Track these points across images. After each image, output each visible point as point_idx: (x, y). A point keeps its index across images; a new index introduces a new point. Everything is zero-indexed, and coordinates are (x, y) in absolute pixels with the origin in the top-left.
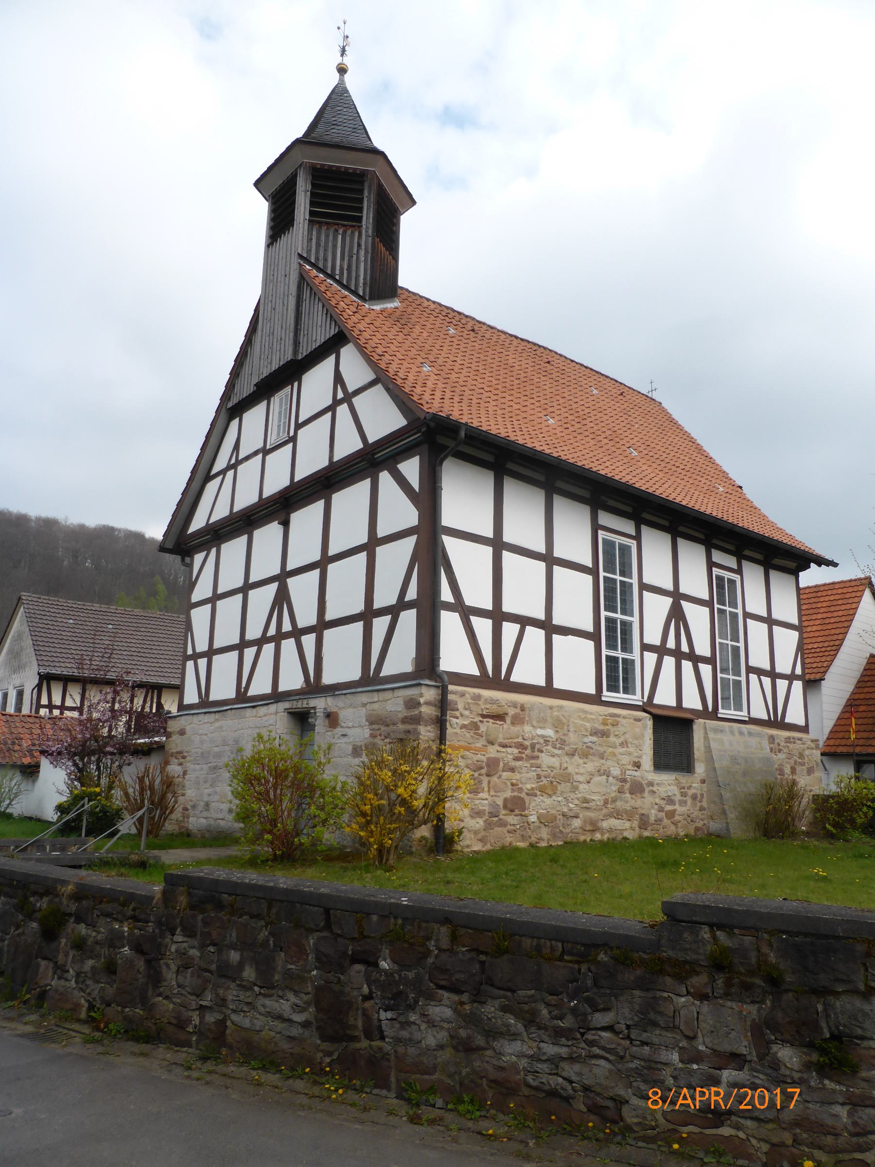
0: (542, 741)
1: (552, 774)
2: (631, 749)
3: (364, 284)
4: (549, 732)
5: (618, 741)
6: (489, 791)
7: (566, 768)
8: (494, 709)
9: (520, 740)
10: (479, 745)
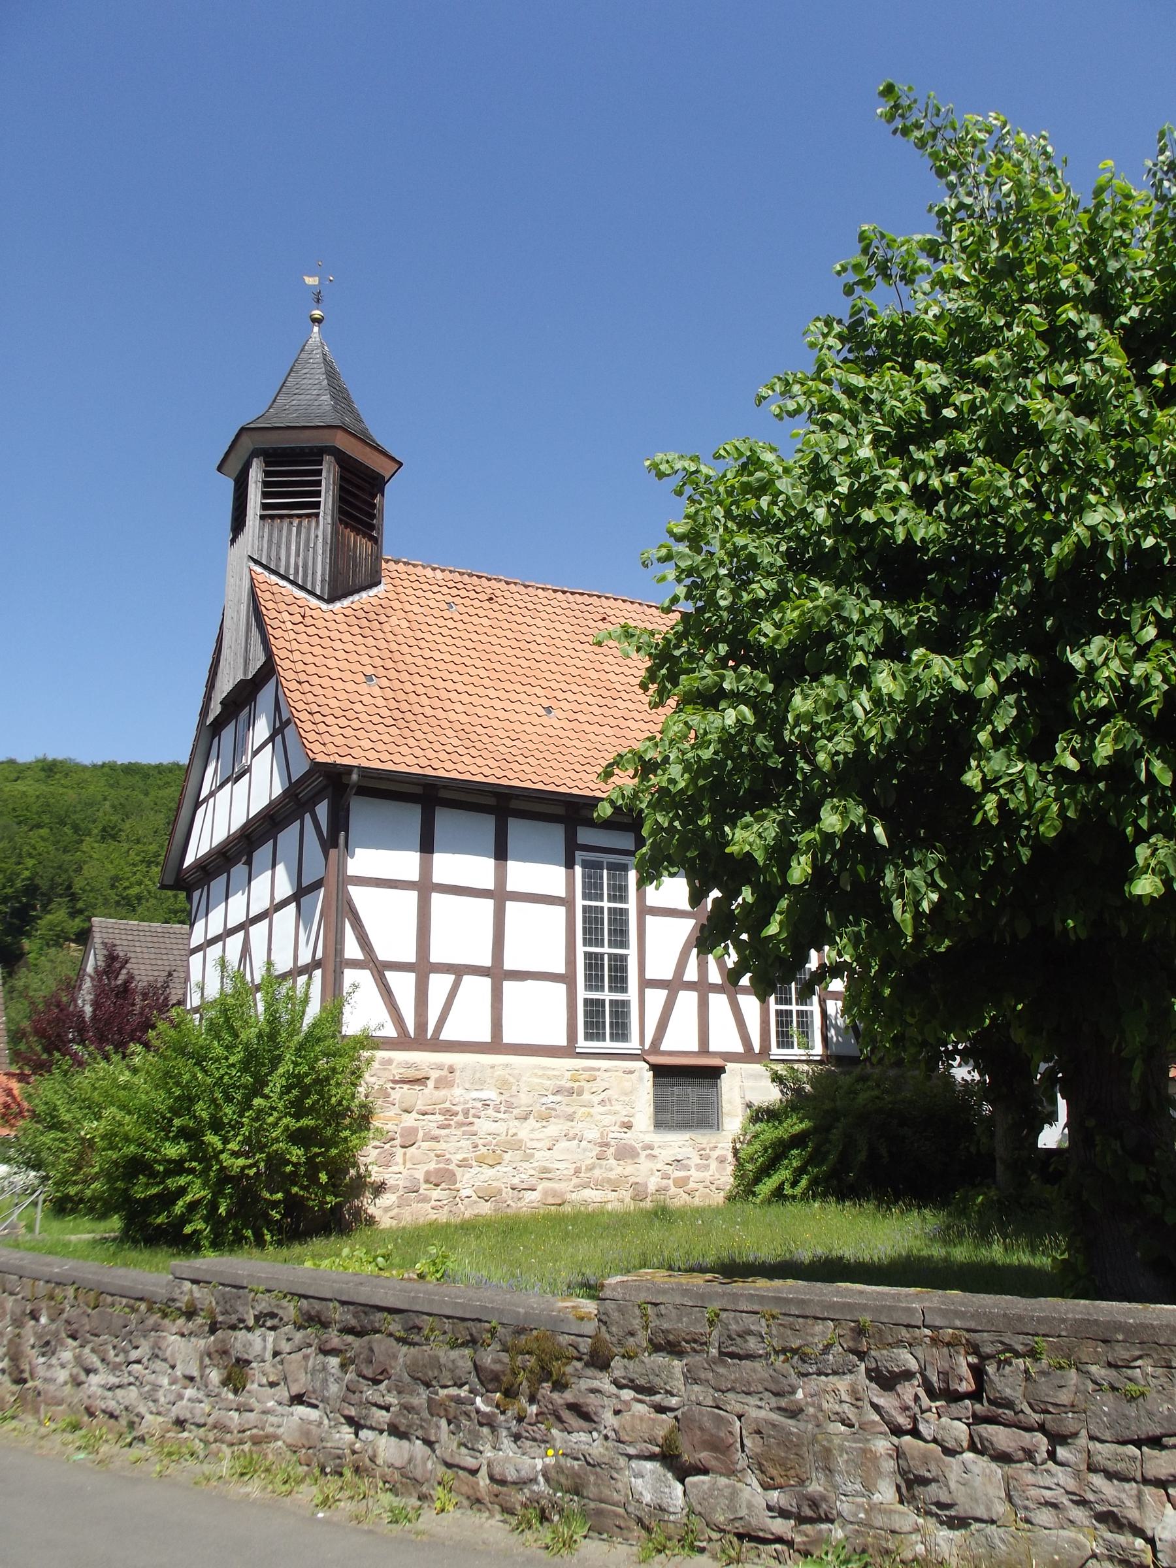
0: (479, 1105)
1: (494, 1142)
2: (617, 1107)
3: (323, 581)
4: (490, 1094)
5: (596, 1099)
6: (404, 1163)
7: (515, 1134)
8: (411, 1074)
9: (447, 1105)
10: (391, 1114)
